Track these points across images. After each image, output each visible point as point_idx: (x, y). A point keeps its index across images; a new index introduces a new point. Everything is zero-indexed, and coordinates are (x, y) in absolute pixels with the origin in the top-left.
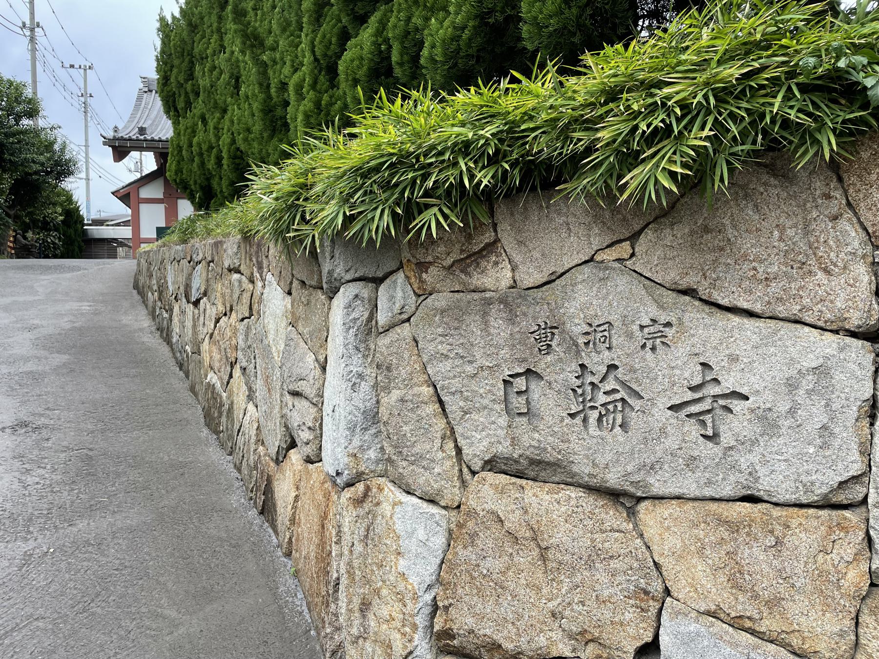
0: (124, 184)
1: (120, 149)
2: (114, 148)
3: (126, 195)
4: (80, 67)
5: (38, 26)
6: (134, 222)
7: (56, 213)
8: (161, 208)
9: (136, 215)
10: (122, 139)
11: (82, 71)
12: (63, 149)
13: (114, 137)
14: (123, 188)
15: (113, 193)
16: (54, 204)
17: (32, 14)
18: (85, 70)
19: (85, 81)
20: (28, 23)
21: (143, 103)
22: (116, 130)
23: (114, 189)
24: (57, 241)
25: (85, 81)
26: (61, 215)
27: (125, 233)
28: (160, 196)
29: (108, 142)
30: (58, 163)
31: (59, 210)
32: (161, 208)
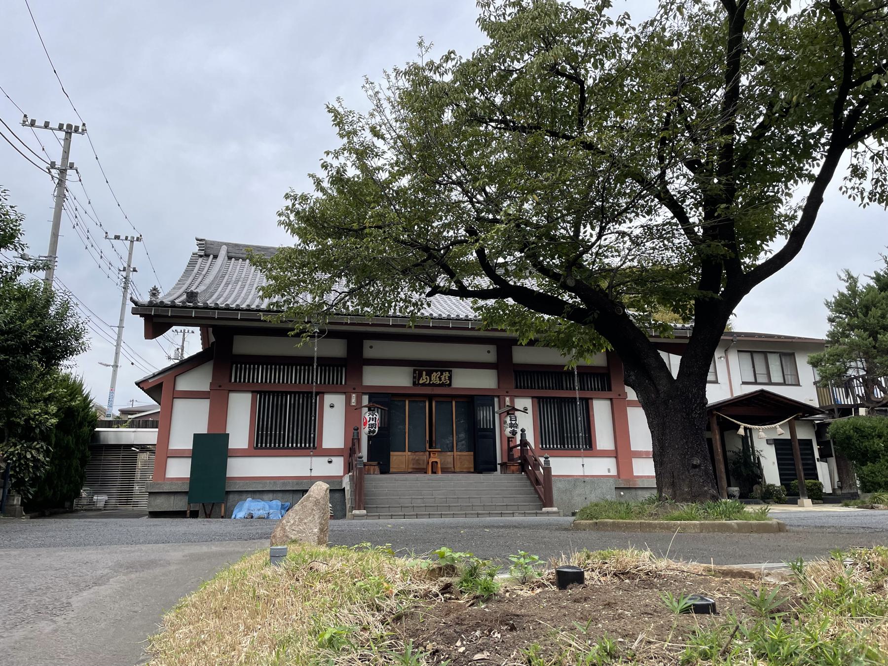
0: (156, 371)
1: (157, 319)
2: (148, 319)
3: (154, 387)
4: (126, 238)
5: (71, 167)
6: (160, 421)
7: (47, 413)
8: (204, 406)
9: (168, 412)
10: (162, 305)
11: (128, 243)
12: (62, 315)
13: (151, 302)
14: (154, 376)
15: (138, 384)
16: (48, 400)
17: (66, 152)
18: (132, 242)
19: (130, 254)
20: (58, 164)
21: (196, 270)
22: (154, 292)
23: (140, 378)
24: (41, 457)
25: (130, 254)
26: (55, 415)
27: (149, 436)
28: (206, 388)
29: (139, 309)
30: (44, 335)
31: (53, 408)
32: (204, 406)
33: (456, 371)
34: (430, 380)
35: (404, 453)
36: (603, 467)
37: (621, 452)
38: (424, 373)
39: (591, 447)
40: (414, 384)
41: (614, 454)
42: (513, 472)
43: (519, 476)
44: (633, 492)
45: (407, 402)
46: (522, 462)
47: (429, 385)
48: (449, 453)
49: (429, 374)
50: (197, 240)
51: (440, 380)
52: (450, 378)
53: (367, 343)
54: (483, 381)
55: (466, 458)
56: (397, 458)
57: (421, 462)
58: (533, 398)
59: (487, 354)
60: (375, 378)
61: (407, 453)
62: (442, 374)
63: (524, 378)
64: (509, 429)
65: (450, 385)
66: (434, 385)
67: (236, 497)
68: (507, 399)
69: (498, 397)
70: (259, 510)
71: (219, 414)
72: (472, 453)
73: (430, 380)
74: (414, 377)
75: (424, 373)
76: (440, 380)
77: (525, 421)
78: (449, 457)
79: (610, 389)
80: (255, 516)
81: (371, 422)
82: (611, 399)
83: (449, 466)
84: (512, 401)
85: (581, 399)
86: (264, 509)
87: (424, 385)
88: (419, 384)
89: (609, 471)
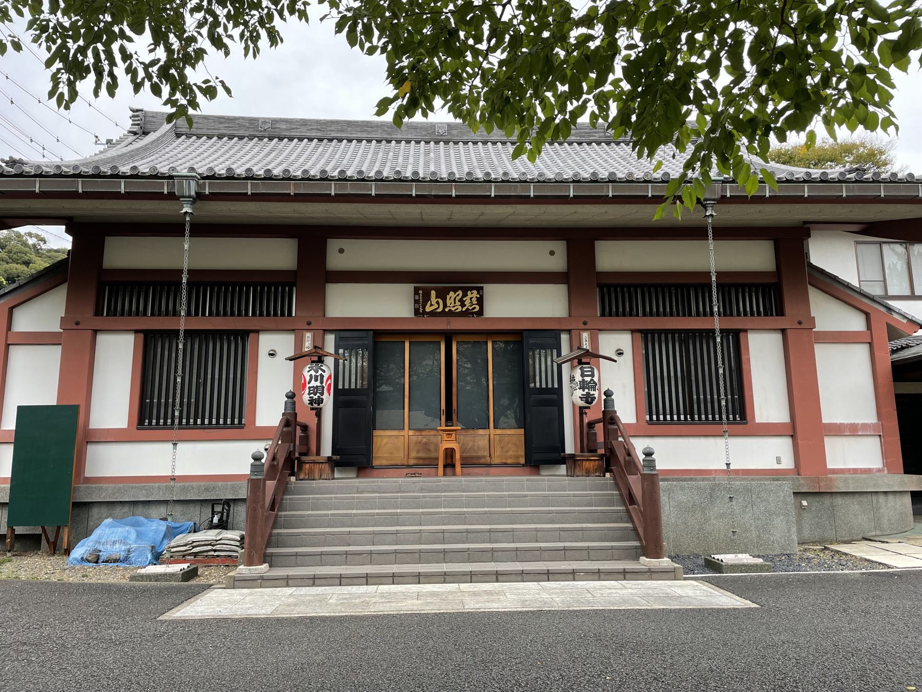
33: (491, 290)
34: (445, 306)
35: (402, 433)
36: (770, 454)
37: (804, 426)
38: (433, 293)
39: (743, 417)
40: (417, 312)
41: (791, 430)
42: (588, 473)
43: (598, 480)
44: (827, 501)
45: (407, 345)
46: (605, 452)
47: (443, 314)
48: (481, 432)
49: (442, 295)
50: (133, 111)
51: (463, 305)
52: (480, 301)
53: (333, 245)
54: (544, 304)
55: (508, 439)
56: (389, 442)
57: (432, 447)
58: (633, 331)
59: (548, 256)
60: (348, 304)
61: (407, 432)
62: (465, 295)
63: (619, 298)
64: (579, 393)
65: (480, 313)
66: (451, 314)
67: (104, 510)
68: (585, 335)
69: (569, 331)
70: (114, 543)
71: (79, 372)
72: (522, 431)
73: (445, 306)
74: (416, 302)
75: (433, 293)
76: (463, 305)
77: (616, 374)
78: (479, 440)
79: (781, 313)
80: (104, 556)
81: (313, 383)
82: (783, 331)
83: (481, 454)
84: (594, 341)
85: (722, 331)
86: (124, 541)
87: (433, 314)
88: (424, 313)
89: (779, 461)
